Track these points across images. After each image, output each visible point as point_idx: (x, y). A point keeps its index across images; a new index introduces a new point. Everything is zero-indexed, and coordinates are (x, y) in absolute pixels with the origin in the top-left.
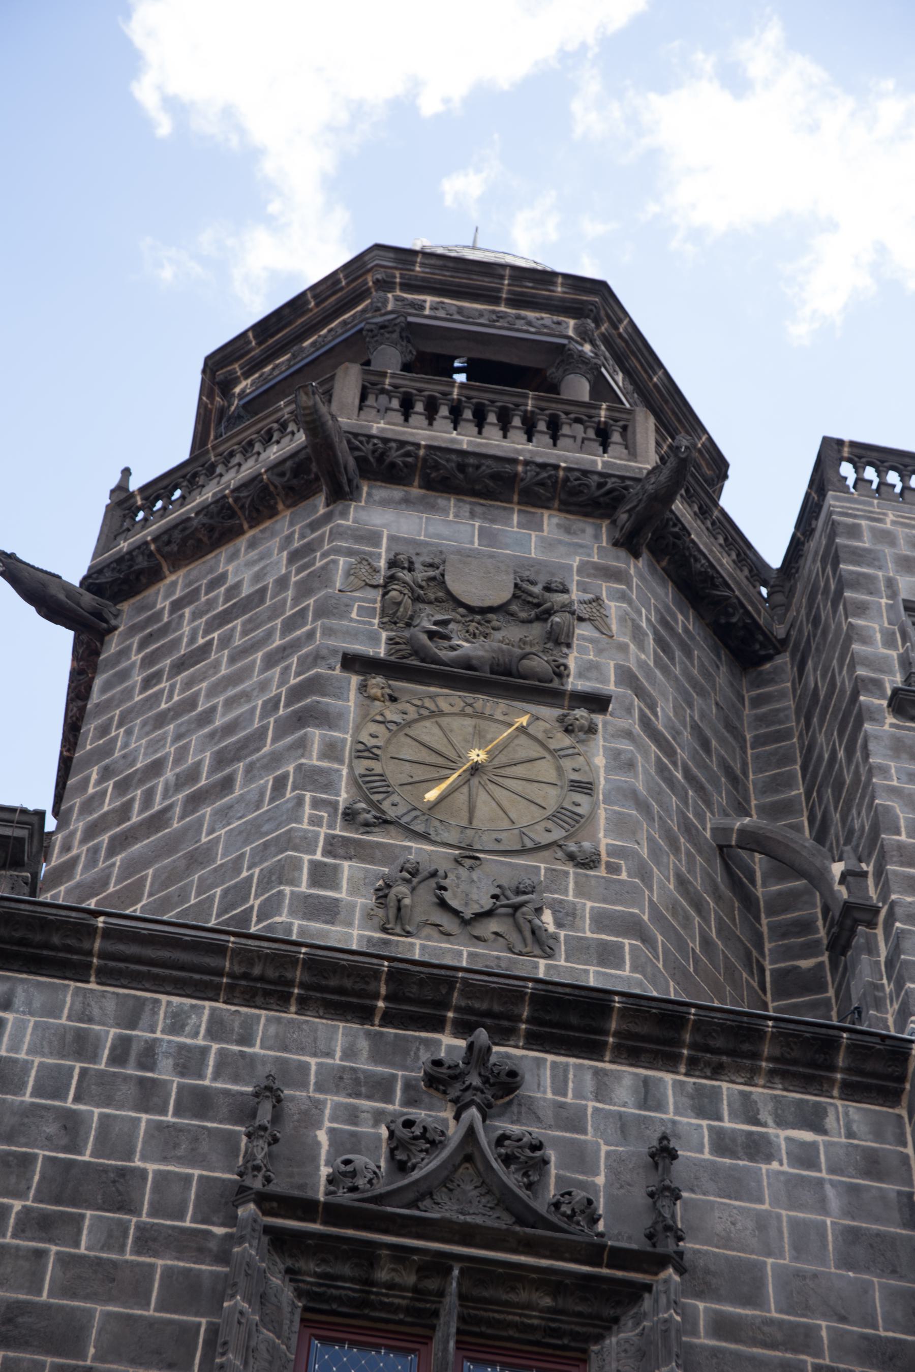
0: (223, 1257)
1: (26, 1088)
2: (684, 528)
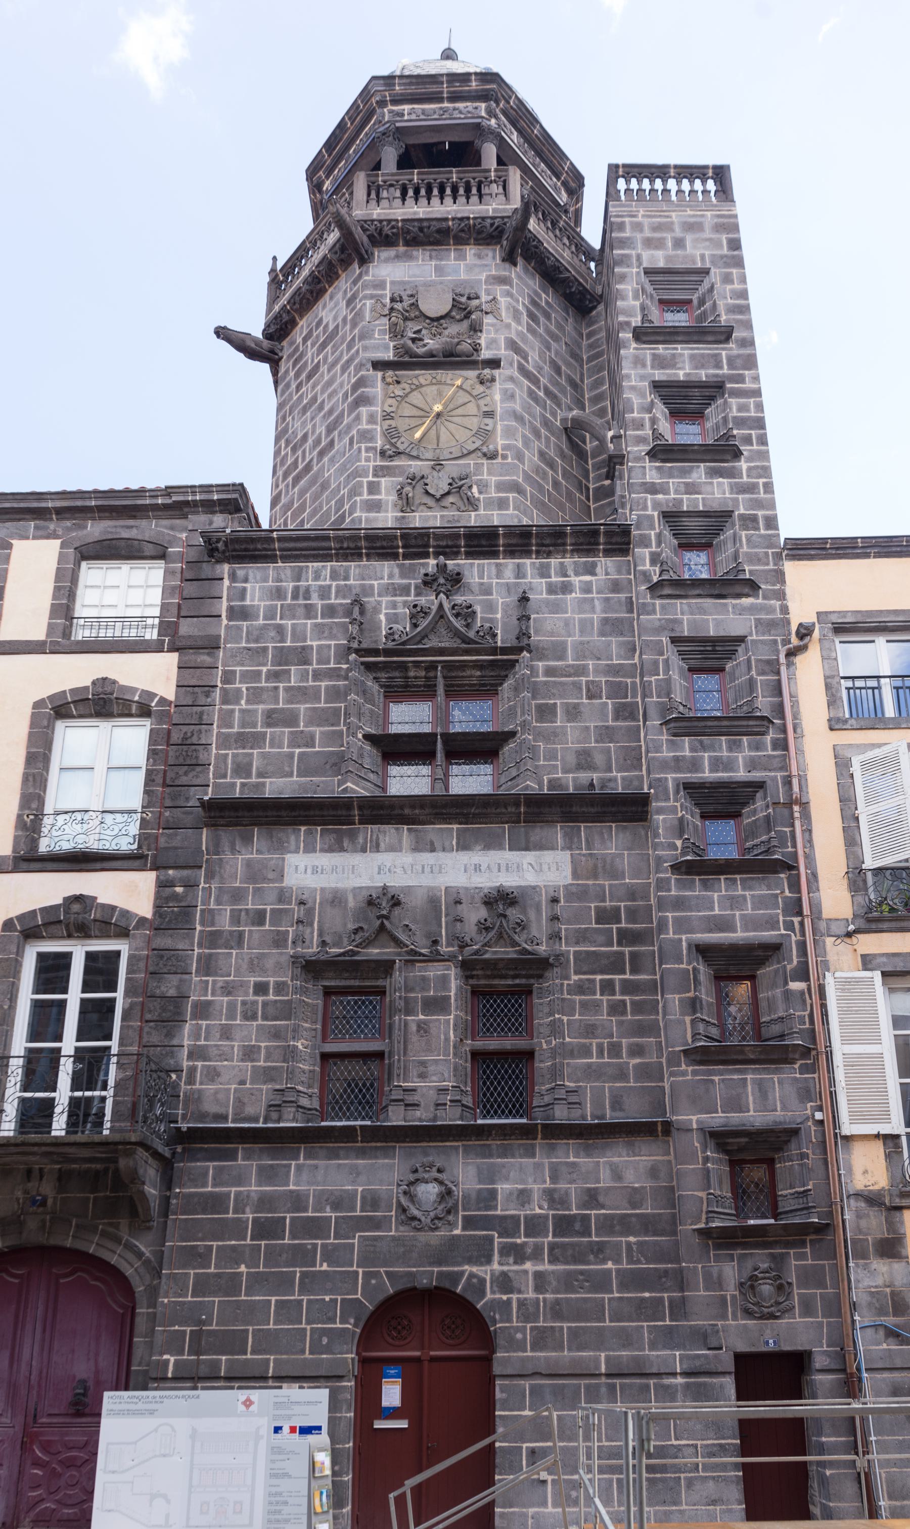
0: (346, 678)
2: (539, 241)
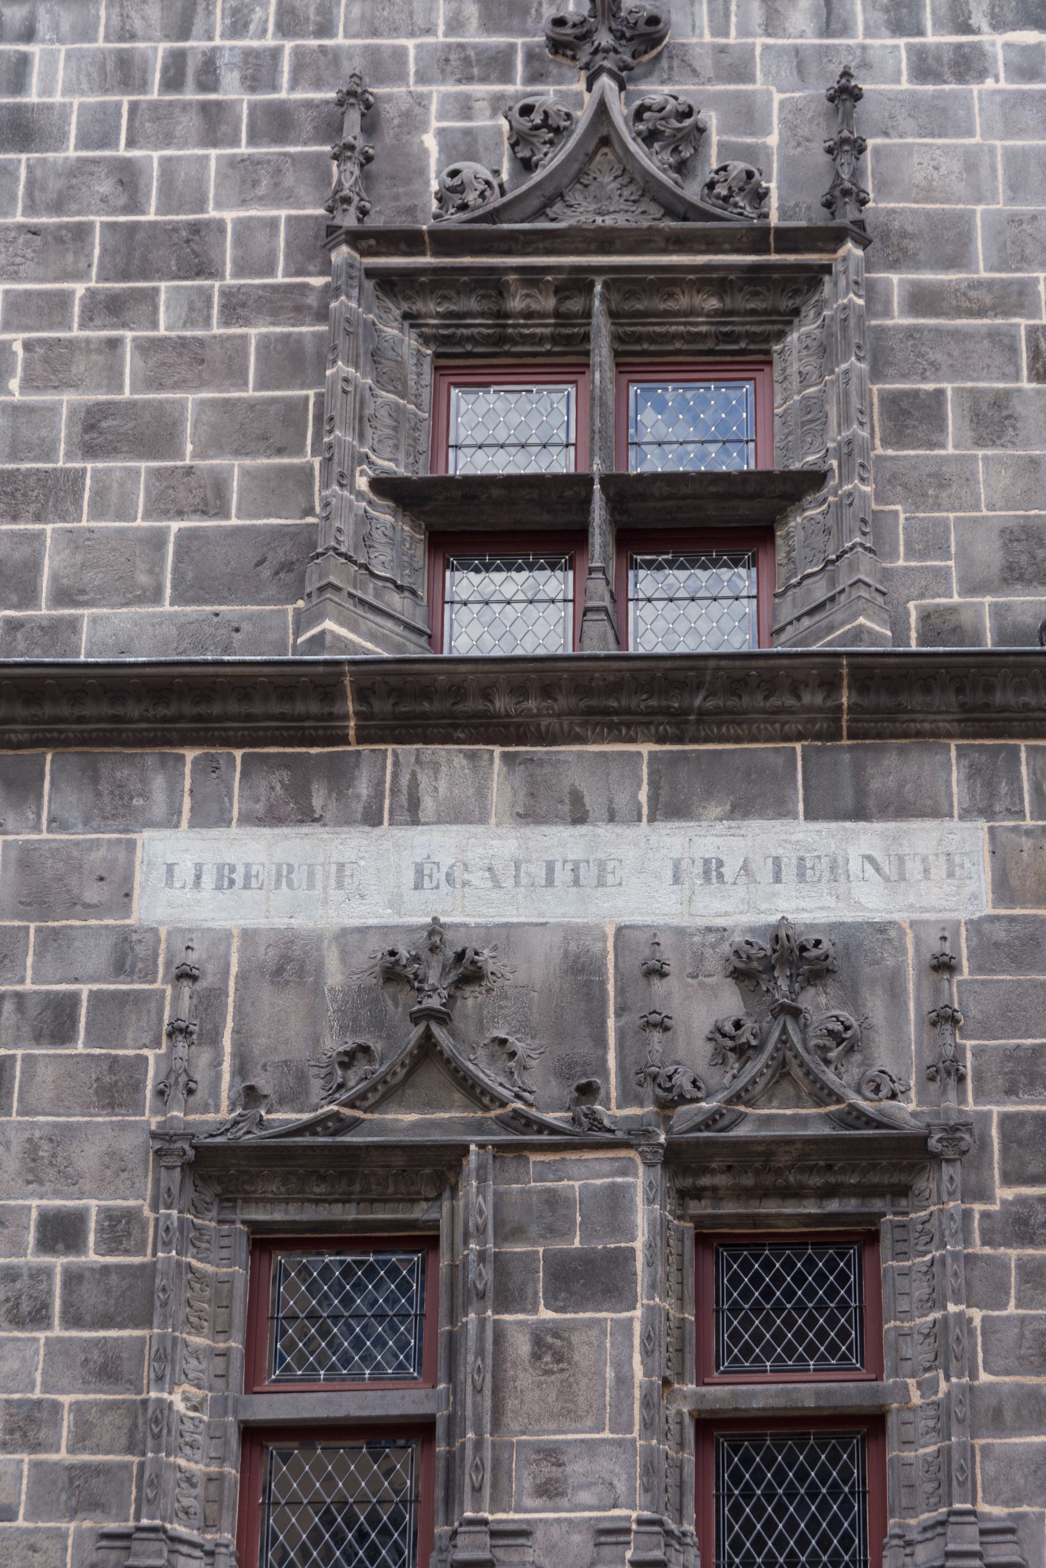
0: (322, 315)
1: (68, 140)
